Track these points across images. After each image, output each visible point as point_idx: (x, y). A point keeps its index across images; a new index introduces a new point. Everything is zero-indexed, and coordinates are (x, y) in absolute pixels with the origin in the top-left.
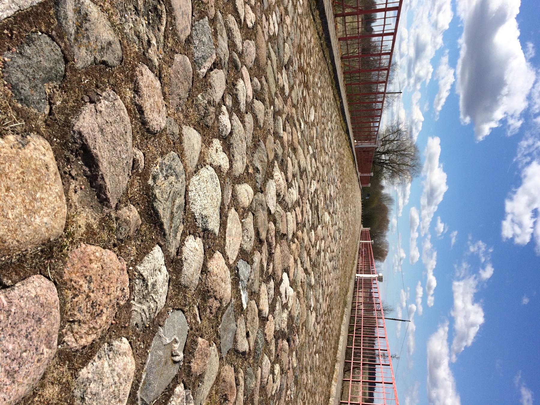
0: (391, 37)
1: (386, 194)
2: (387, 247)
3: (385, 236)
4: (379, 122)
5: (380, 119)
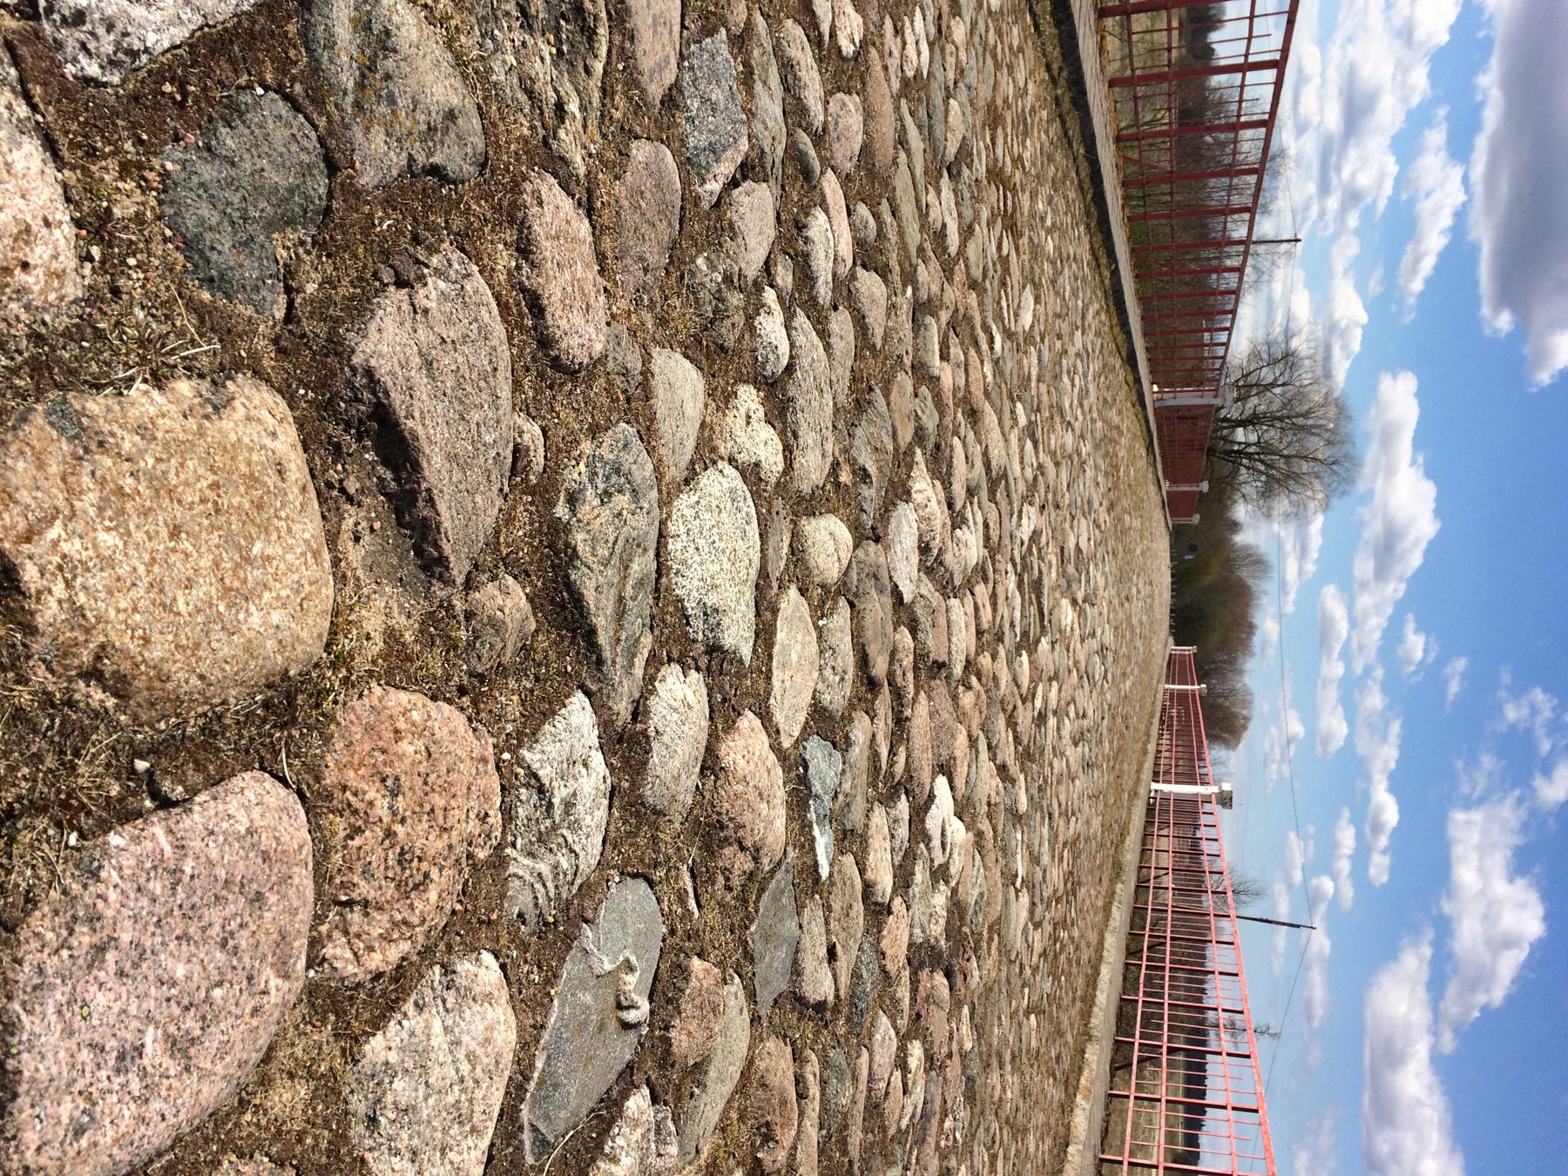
0: (1270, 75)
2: (1247, 703)
3: (1241, 672)
4: (1230, 330)
5: (1233, 320)
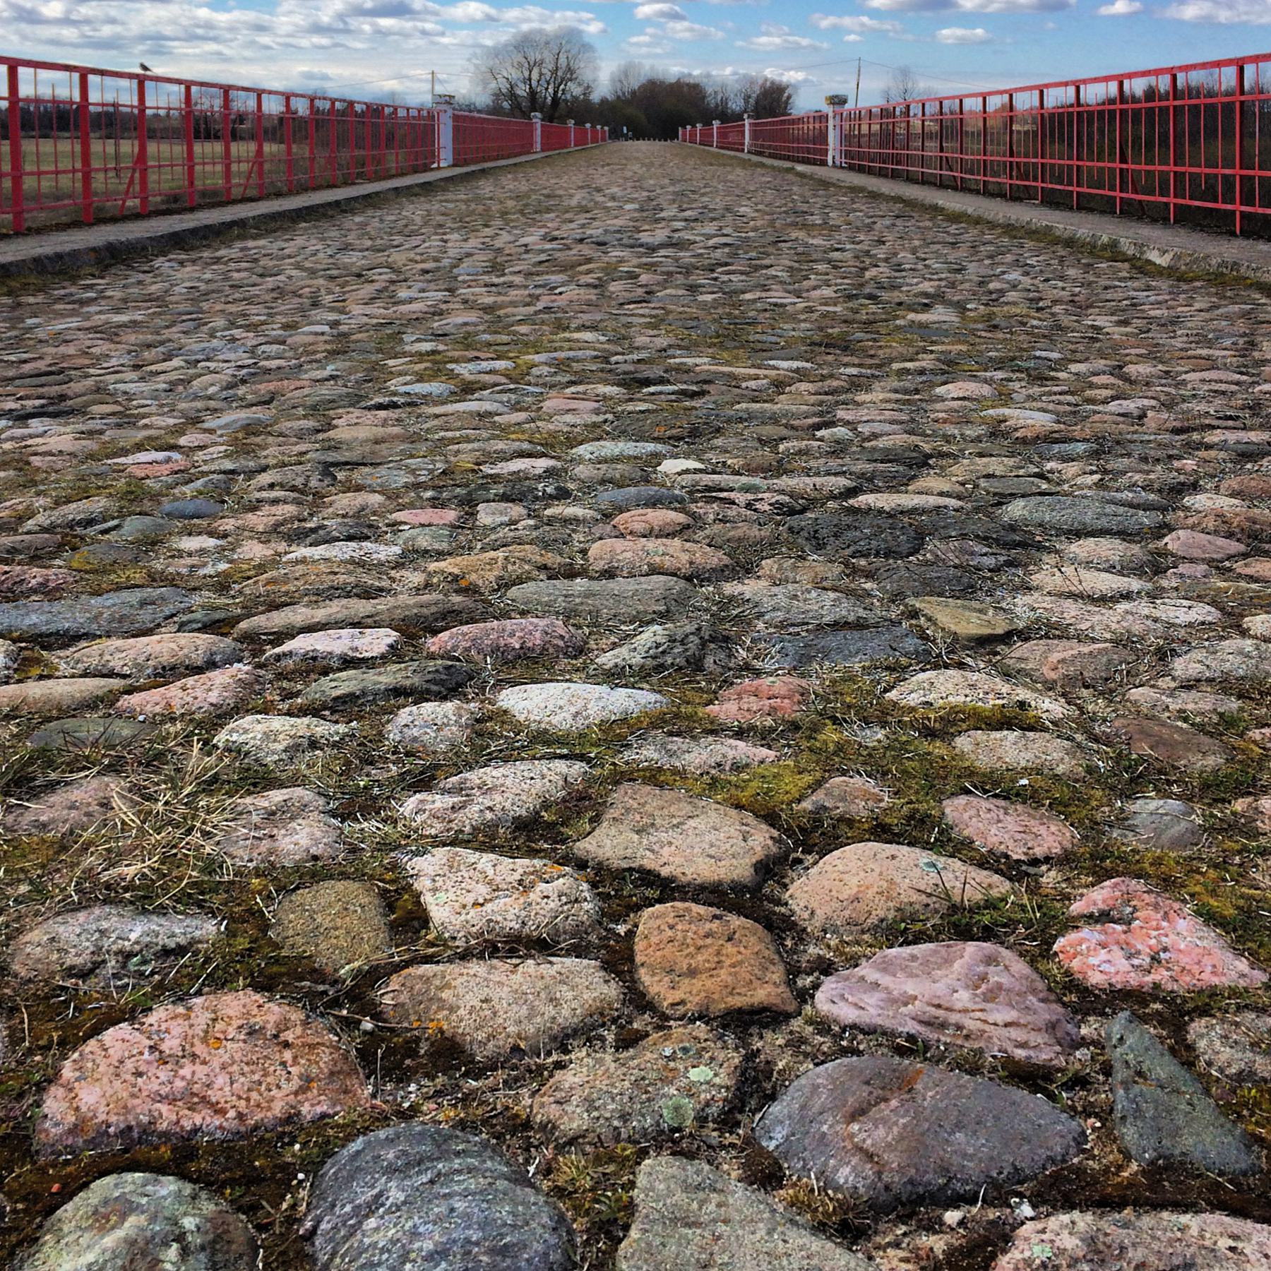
1: (613, 80)
2: (752, 82)
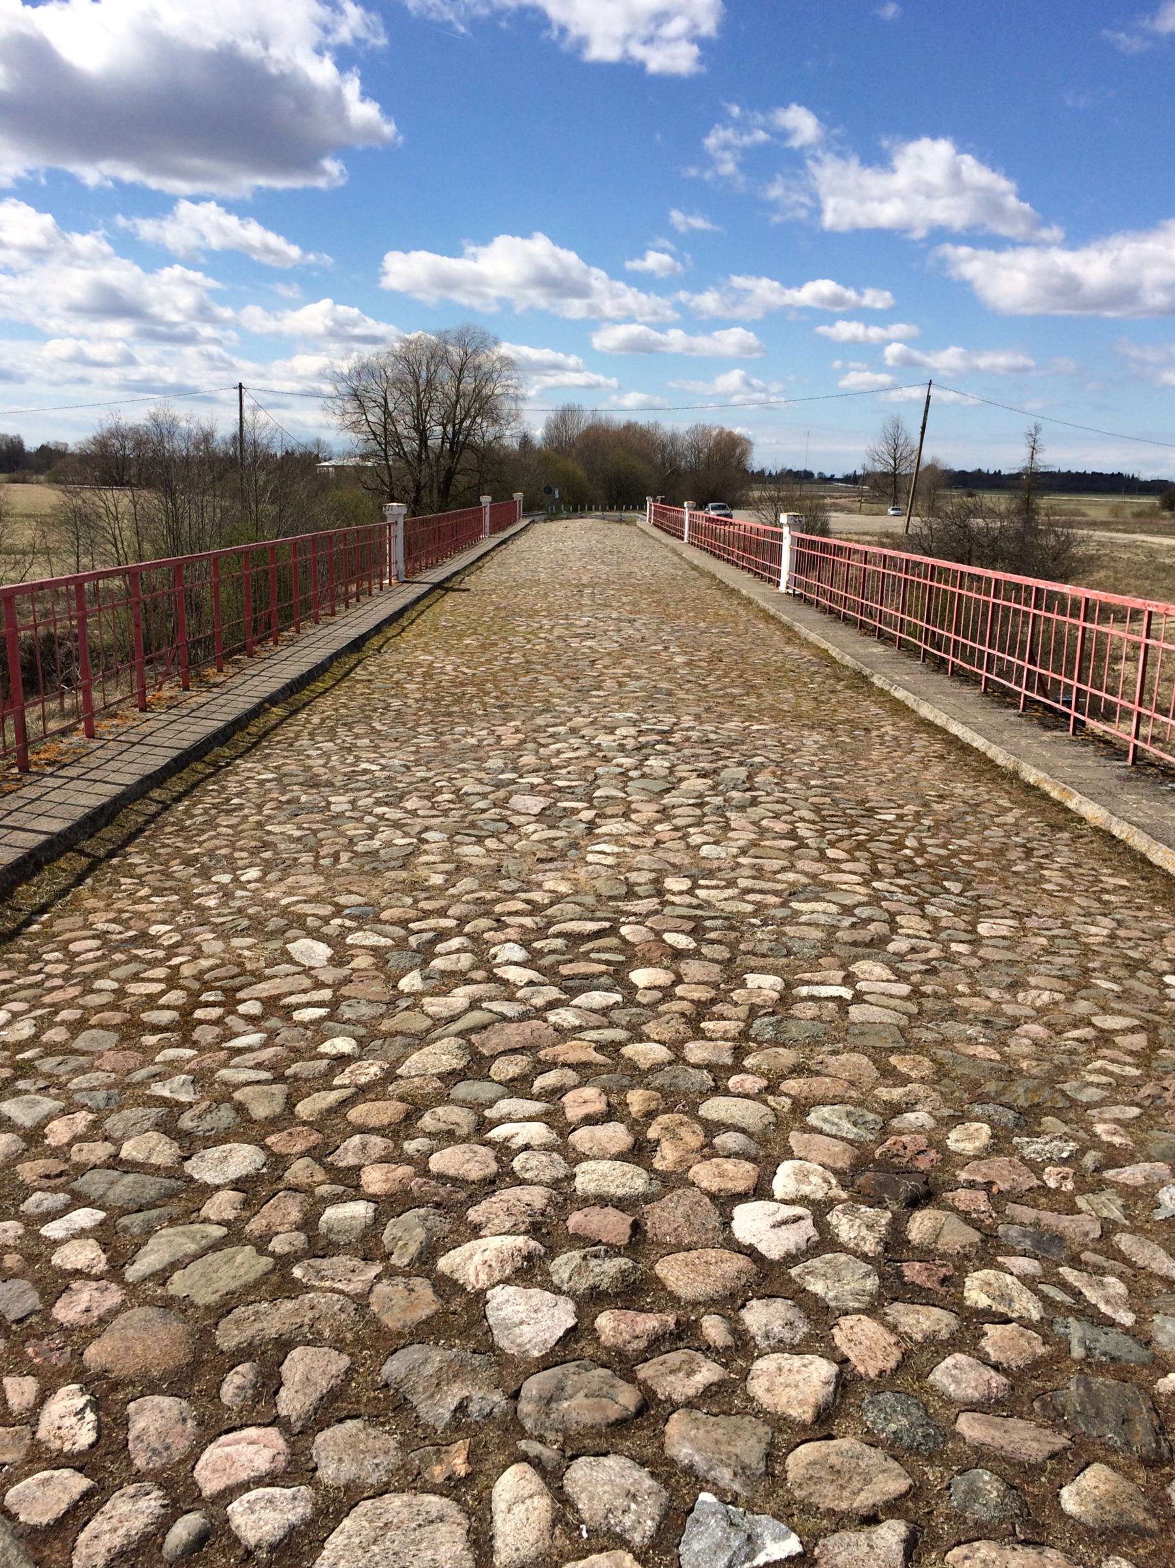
1: (548, 427)
2: (705, 432)
3: (674, 438)
